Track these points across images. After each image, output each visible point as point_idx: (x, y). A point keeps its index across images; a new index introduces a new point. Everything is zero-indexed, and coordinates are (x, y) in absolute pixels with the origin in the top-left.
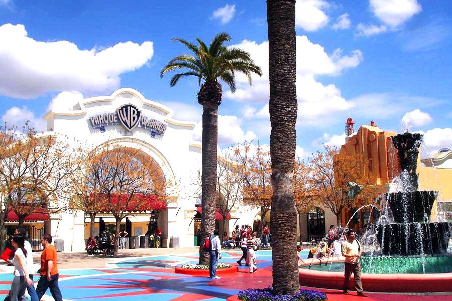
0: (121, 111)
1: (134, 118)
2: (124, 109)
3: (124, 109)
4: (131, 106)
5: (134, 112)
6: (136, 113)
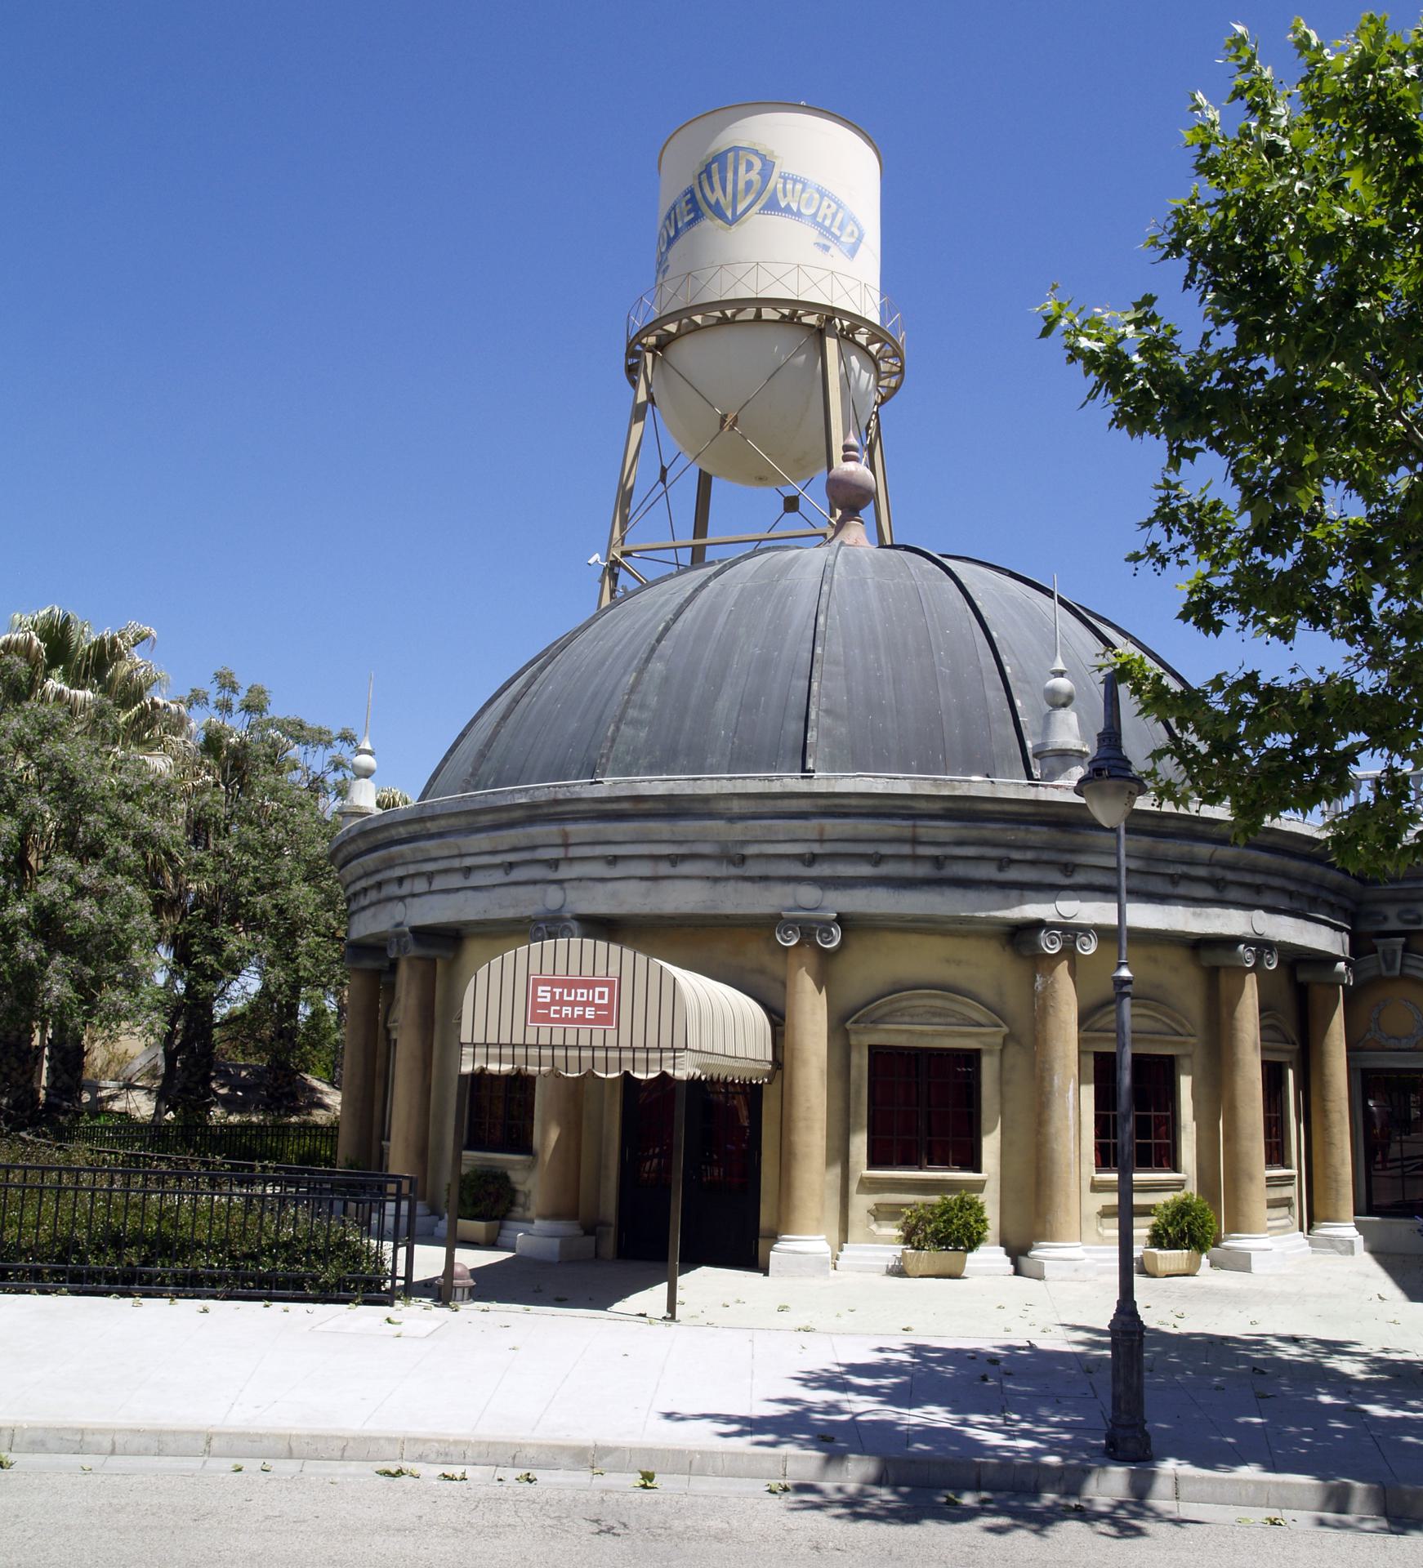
0: (704, 176)
3: (715, 166)
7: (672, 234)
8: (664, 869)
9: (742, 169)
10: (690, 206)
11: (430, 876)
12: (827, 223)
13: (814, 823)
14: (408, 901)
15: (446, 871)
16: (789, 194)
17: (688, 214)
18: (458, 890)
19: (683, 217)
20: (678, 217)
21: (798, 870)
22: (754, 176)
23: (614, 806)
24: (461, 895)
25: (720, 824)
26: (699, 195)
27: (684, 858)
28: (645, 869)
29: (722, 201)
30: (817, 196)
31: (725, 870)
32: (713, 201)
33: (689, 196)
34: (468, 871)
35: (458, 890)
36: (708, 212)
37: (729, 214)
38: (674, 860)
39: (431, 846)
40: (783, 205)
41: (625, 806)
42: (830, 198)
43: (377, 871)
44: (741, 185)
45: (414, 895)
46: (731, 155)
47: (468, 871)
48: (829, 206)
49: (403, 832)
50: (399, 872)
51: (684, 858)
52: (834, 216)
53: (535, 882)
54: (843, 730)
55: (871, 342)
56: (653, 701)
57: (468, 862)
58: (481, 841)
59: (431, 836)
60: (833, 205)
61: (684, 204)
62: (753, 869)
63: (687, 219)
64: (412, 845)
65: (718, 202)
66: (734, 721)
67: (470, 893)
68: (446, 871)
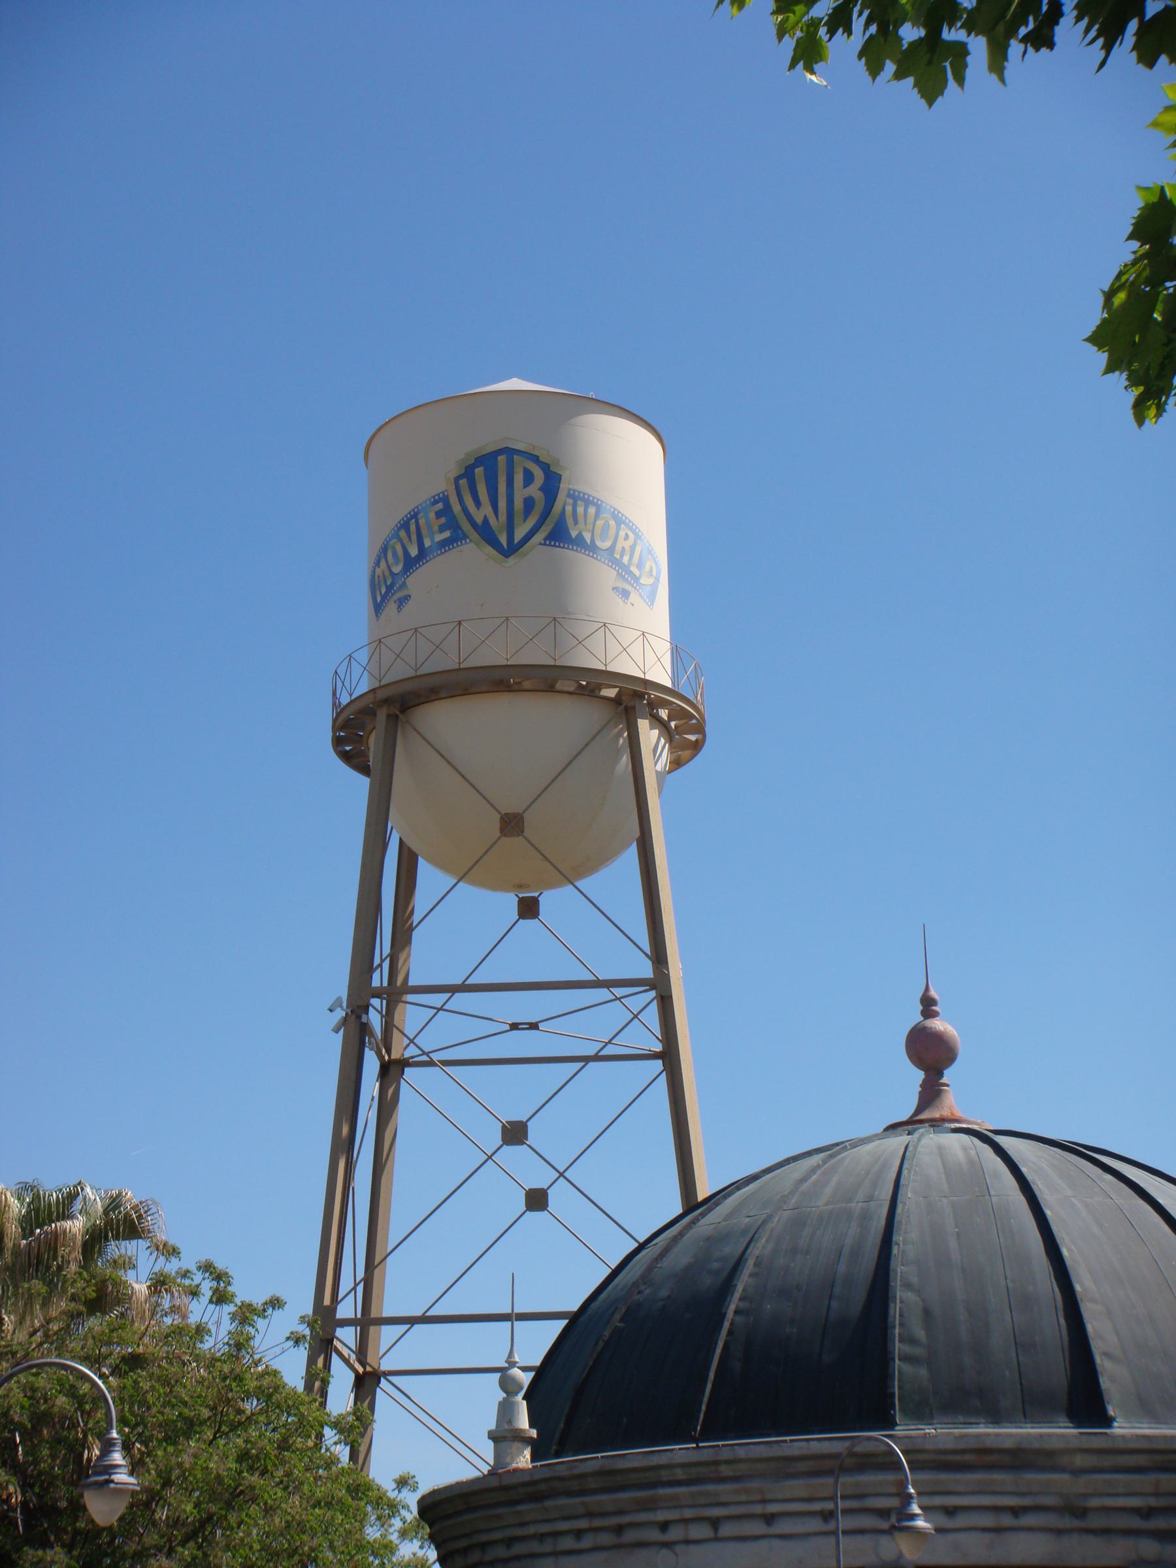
0: (463, 482)
1: (529, 504)
2: (479, 471)
3: (479, 471)
4: (510, 452)
5: (529, 478)
6: (538, 474)
7: (414, 551)
8: (1007, 1520)
9: (519, 479)
10: (443, 520)
11: (715, 1523)
12: (626, 559)
13: (1152, 1477)
14: (679, 1548)
15: (739, 1517)
16: (581, 520)
17: (441, 531)
18: (757, 1538)
19: (432, 535)
20: (424, 532)
21: (1136, 1522)
22: (534, 491)
23: (958, 1458)
24: (763, 1544)
25: (1066, 1477)
26: (457, 508)
27: (1025, 1510)
28: (988, 1520)
29: (492, 521)
30: (612, 523)
31: (1068, 1522)
32: (479, 520)
33: (440, 506)
34: (769, 1519)
35: (757, 1538)
36: (473, 534)
37: (503, 539)
38: (1015, 1511)
39: (724, 1490)
40: (574, 534)
41: (968, 1457)
42: (627, 525)
43: (621, 1512)
44: (518, 504)
45: (687, 1542)
46: (502, 459)
47: (769, 1519)
48: (627, 537)
49: (680, 1474)
50: (661, 1516)
51: (1025, 1510)
52: (633, 548)
53: (861, 1532)
54: (709, 1281)
55: (670, 718)
56: (920, 1334)
57: (773, 1508)
58: (797, 1487)
59: (722, 1480)
60: (631, 535)
61: (432, 515)
62: (1095, 1522)
63: (439, 537)
64: (694, 1489)
65: (486, 520)
66: (1015, 1363)
67: (777, 1543)
68: (739, 1517)
